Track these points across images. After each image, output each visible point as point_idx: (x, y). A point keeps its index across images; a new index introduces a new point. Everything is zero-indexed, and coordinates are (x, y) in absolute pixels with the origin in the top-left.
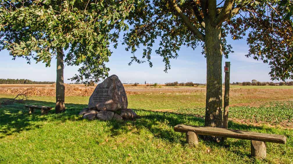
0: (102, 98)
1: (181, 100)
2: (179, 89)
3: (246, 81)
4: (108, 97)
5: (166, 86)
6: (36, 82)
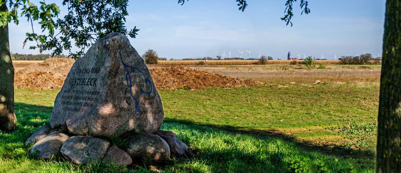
0: (81, 101)
1: (363, 102)
2: (370, 73)
3: (23, 46)
4: (95, 97)
5: (341, 64)
6: (21, 55)
